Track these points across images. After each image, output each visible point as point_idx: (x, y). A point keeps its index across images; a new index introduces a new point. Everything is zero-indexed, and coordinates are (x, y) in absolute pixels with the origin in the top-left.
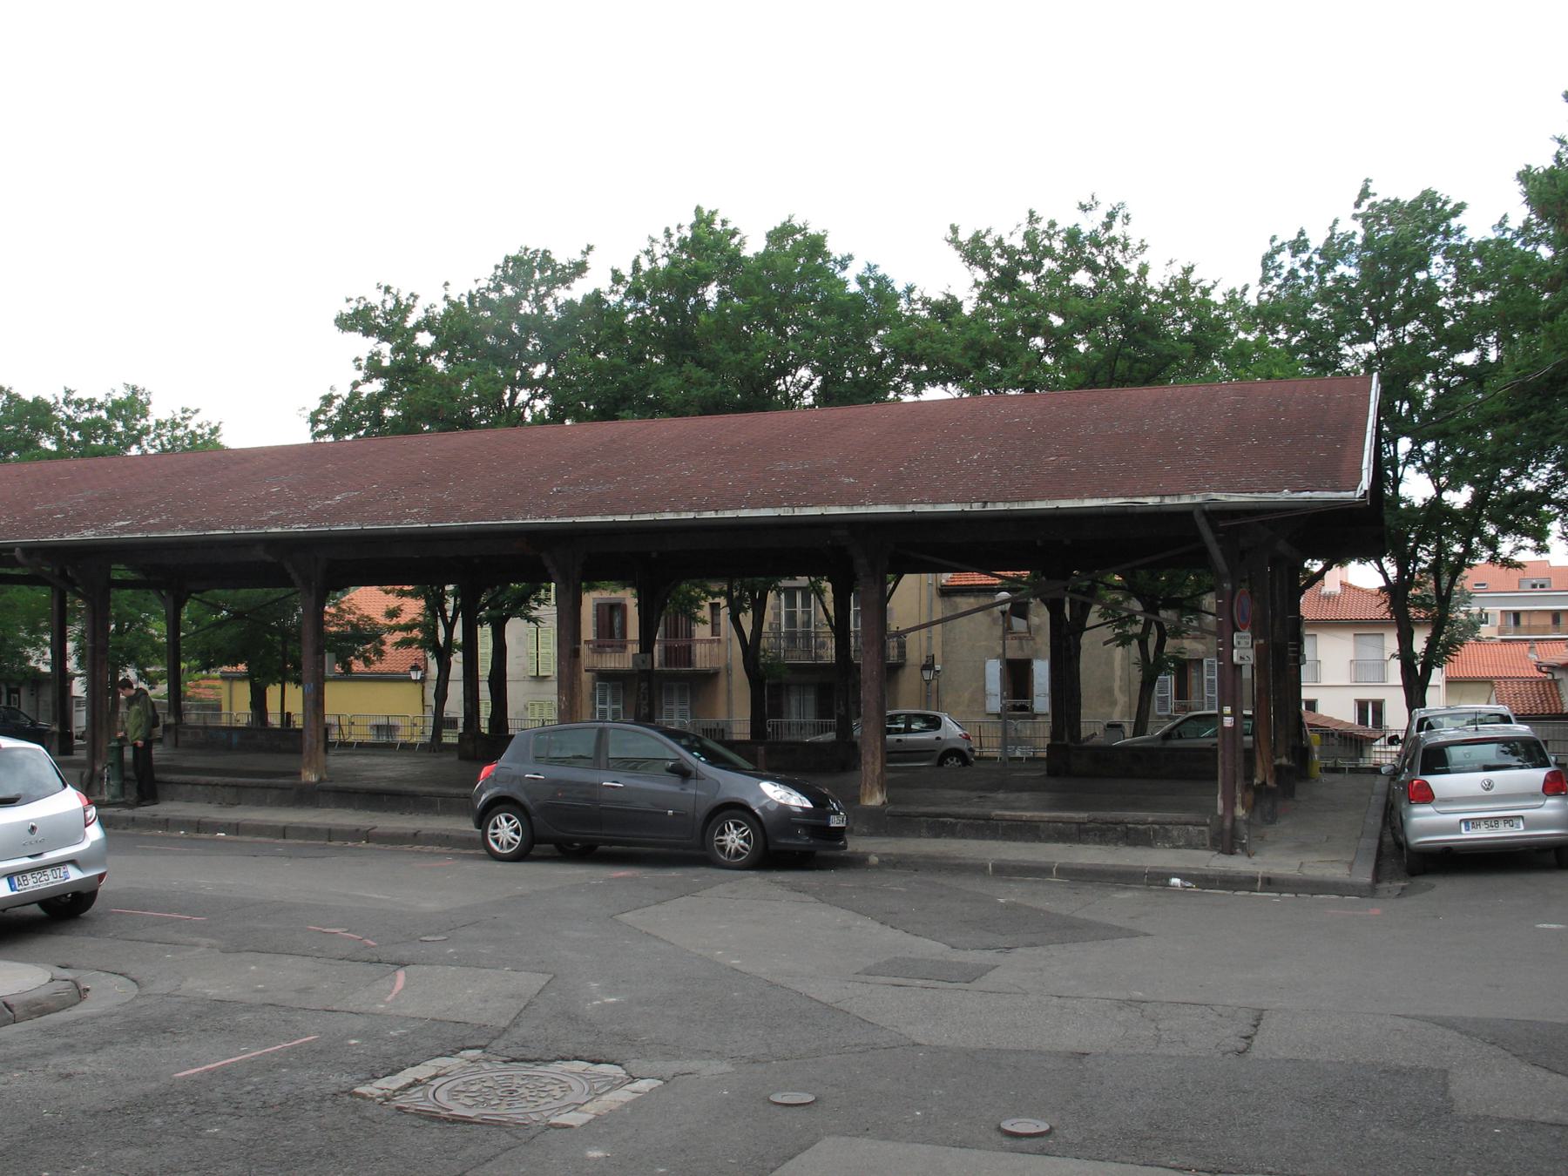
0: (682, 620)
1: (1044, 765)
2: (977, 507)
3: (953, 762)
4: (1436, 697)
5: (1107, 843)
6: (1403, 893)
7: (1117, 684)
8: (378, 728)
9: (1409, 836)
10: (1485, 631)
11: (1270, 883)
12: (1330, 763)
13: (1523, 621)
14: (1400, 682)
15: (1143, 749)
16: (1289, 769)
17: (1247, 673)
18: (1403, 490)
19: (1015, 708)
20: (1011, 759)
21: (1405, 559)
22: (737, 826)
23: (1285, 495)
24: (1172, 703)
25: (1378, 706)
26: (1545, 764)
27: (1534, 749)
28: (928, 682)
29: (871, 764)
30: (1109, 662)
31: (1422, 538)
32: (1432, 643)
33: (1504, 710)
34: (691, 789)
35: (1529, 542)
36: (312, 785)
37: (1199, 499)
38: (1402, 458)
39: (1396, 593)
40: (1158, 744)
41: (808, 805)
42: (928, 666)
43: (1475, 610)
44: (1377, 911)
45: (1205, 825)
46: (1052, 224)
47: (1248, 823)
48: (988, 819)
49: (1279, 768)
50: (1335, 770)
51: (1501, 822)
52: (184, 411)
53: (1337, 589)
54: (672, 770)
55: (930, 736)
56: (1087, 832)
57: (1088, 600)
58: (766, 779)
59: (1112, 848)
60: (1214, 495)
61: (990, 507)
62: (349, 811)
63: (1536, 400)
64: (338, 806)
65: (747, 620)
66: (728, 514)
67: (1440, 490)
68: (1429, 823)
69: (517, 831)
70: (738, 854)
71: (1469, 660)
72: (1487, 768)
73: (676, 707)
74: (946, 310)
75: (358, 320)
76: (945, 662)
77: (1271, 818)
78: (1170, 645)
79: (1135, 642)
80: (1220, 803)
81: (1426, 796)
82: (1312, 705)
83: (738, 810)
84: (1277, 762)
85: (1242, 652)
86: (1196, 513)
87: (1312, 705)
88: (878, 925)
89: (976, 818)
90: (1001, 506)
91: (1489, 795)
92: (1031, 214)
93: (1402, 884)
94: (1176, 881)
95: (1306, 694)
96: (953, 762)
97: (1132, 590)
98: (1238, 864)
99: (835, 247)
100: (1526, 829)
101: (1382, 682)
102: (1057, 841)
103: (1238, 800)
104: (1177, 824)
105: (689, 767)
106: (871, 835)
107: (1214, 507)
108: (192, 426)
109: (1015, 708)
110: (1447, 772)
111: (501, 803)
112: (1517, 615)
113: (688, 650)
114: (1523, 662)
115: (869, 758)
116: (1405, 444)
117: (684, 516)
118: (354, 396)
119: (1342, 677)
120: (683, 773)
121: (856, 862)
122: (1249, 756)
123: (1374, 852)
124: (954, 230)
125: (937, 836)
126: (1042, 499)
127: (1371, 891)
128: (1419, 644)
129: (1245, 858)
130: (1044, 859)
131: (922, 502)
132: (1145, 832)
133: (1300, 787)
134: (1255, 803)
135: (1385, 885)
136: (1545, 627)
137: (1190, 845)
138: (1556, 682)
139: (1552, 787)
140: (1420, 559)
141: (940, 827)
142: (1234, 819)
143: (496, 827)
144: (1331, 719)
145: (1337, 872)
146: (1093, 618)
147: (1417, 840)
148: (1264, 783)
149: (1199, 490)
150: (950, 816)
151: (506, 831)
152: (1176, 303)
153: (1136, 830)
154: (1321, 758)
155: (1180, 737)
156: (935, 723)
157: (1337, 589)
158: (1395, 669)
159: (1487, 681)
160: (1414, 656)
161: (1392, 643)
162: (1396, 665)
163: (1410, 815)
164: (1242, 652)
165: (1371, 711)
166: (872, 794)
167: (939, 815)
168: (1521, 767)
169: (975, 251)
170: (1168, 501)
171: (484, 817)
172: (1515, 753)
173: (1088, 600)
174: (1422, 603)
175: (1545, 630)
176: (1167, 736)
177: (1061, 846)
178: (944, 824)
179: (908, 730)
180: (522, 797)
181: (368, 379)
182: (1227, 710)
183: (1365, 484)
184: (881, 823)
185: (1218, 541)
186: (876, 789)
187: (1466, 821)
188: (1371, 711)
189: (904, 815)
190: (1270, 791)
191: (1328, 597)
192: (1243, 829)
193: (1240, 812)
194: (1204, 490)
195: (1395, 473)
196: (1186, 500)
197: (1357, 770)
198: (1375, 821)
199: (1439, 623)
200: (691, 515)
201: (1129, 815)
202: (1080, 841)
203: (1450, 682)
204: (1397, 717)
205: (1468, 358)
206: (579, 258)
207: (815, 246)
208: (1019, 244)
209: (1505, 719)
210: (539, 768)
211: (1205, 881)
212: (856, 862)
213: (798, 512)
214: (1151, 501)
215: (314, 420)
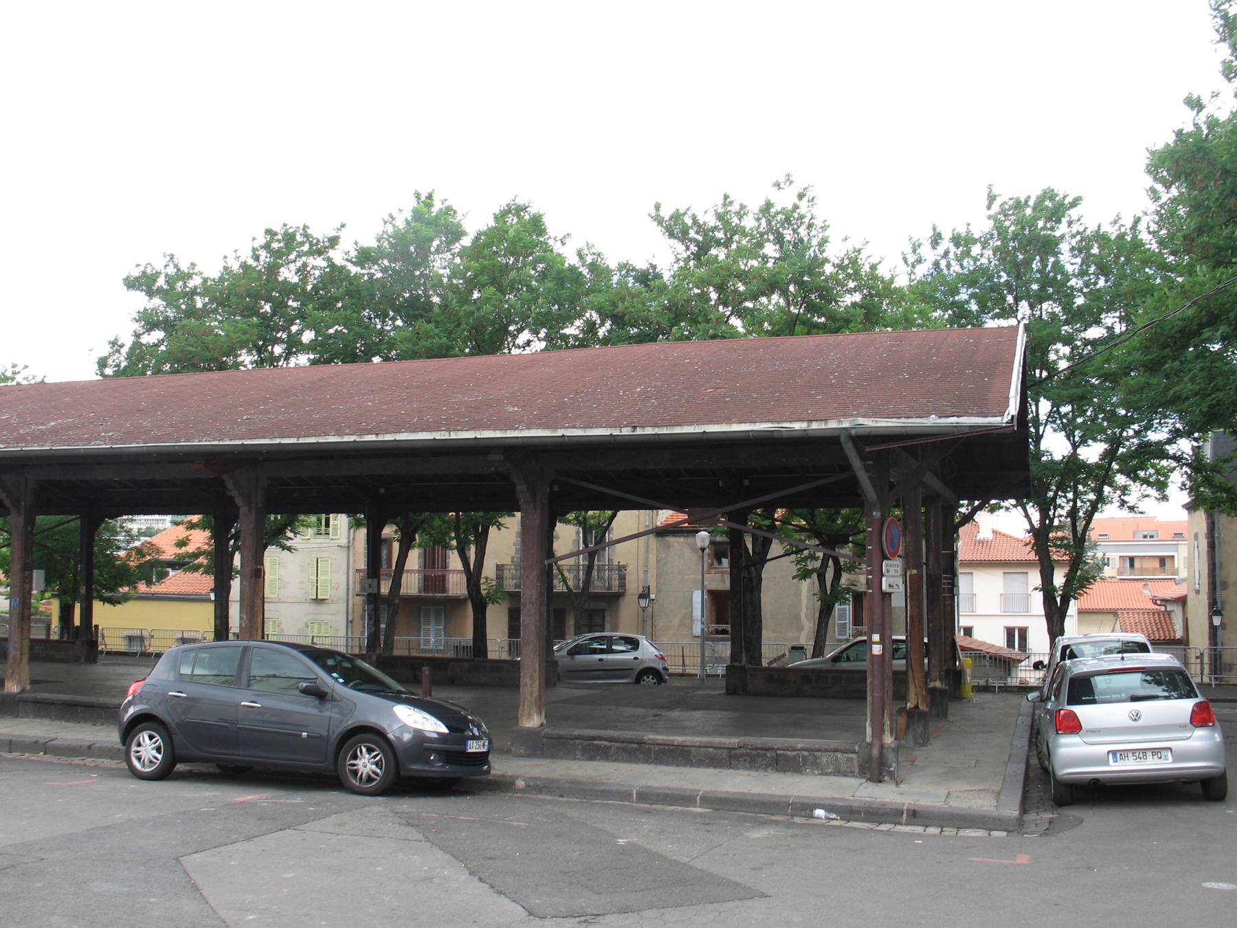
0: (439, 549)
1: (723, 683)
2: (626, 431)
3: (649, 680)
4: (1072, 627)
5: (757, 769)
6: (1050, 829)
7: (804, 612)
8: (130, 639)
9: (1057, 768)
10: (1108, 572)
11: (915, 816)
12: (982, 683)
13: (1137, 564)
14: (1043, 613)
15: (812, 671)
16: (942, 692)
17: (898, 601)
18: (1044, 445)
19: (717, 632)
20: (708, 676)
21: (1046, 507)
22: (370, 750)
23: (932, 421)
24: (850, 629)
25: (1023, 632)
26: (1190, 694)
27: (1178, 678)
28: (644, 609)
29: (530, 683)
30: (797, 594)
31: (1062, 487)
32: (1070, 578)
33: (1140, 638)
34: (330, 712)
35: (1152, 492)
36: (13, 696)
37: (846, 424)
38: (1043, 417)
39: (1040, 536)
40: (828, 666)
41: (444, 730)
42: (644, 595)
43: (1099, 555)
44: (1023, 859)
45: (854, 752)
46: (742, 207)
47: (897, 750)
48: (641, 743)
49: (933, 691)
50: (986, 689)
51: (1149, 754)
52: (14, 366)
53: (990, 536)
54: (306, 691)
55: (630, 656)
56: (737, 757)
57: (768, 535)
58: (398, 698)
59: (761, 773)
60: (861, 420)
61: (639, 431)
62: (46, 721)
63: (1167, 351)
64: (36, 716)
65: (472, 552)
66: (388, 437)
67: (1075, 446)
68: (1075, 754)
69: (158, 750)
70: (370, 779)
71: (1096, 595)
72: (1135, 699)
73: (432, 627)
74: (647, 278)
75: (143, 282)
76: (658, 592)
77: (924, 741)
78: (845, 579)
79: (815, 576)
80: (869, 731)
81: (1074, 726)
82: (968, 631)
83: (371, 735)
84: (931, 685)
85: (891, 580)
86: (843, 439)
87: (968, 631)
88: (464, 876)
89: (631, 741)
90: (649, 431)
91: (1136, 727)
92: (726, 197)
93: (1049, 816)
94: (820, 812)
95: (963, 621)
96: (649, 680)
97: (814, 531)
98: (884, 794)
99: (554, 228)
100: (1175, 761)
101: (1026, 613)
102: (708, 766)
103: (887, 728)
104: (826, 750)
105: (326, 690)
106: (528, 756)
107: (861, 432)
108: (19, 378)
109: (717, 632)
110: (1094, 702)
111: (143, 720)
112: (1132, 560)
113: (443, 579)
114: (1141, 597)
115: (528, 680)
116: (1045, 406)
117: (346, 439)
118: (137, 345)
119: (993, 607)
120: (318, 694)
121: (502, 786)
122: (900, 680)
123: (1021, 779)
124: (657, 207)
125: (591, 759)
126: (690, 424)
127: (1017, 827)
128: (1059, 579)
129: (892, 787)
130: (690, 787)
131: (574, 427)
132: (795, 758)
133: (953, 707)
134: (907, 727)
135: (1031, 816)
136: (1155, 569)
137: (839, 772)
138: (1169, 613)
139: (1200, 718)
140: (1060, 506)
141: (594, 751)
142: (882, 747)
143: (139, 745)
144: (984, 643)
145: (984, 804)
146: (776, 548)
147: (1065, 772)
148: (917, 707)
149: (846, 416)
150: (605, 739)
151: (148, 748)
152: (849, 276)
153: (786, 756)
154: (973, 677)
155: (848, 659)
156: (634, 644)
157: (990, 536)
158: (1037, 601)
159: (1114, 613)
160: (1054, 589)
161: (1035, 578)
162: (1039, 596)
163: (1057, 746)
164: (891, 580)
165: (1017, 636)
166: (530, 716)
167: (594, 738)
168: (1167, 698)
169: (675, 227)
170: (815, 426)
171: (130, 730)
172: (1159, 683)
173: (768, 535)
174: (1061, 544)
175: (1154, 572)
176: (836, 659)
177: (711, 771)
178: (598, 747)
179: (610, 651)
180: (159, 711)
181: (149, 330)
182: (876, 637)
183: (1013, 408)
184: (538, 745)
185: (867, 469)
186: (535, 710)
187: (1114, 753)
188: (1017, 636)
189: (560, 737)
190: (922, 715)
191: (982, 542)
192: (891, 756)
193: (888, 739)
194: (852, 415)
195: (1037, 431)
196: (833, 424)
197: (1006, 689)
198: (1022, 743)
199: (1076, 563)
200: (352, 438)
201: (778, 741)
202: (730, 767)
203: (1081, 612)
204: (1039, 642)
205: (1094, 333)
206: (333, 234)
207: (536, 225)
208: (712, 221)
209: (1142, 648)
210: (182, 686)
211: (849, 812)
212: (502, 786)
213: (453, 436)
214: (797, 426)
215: (103, 363)
